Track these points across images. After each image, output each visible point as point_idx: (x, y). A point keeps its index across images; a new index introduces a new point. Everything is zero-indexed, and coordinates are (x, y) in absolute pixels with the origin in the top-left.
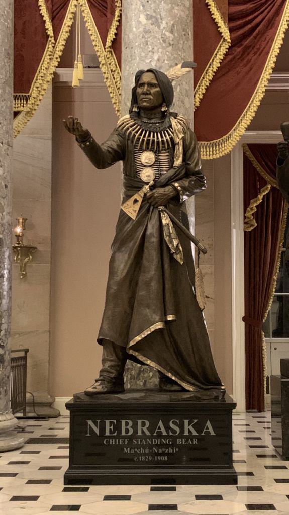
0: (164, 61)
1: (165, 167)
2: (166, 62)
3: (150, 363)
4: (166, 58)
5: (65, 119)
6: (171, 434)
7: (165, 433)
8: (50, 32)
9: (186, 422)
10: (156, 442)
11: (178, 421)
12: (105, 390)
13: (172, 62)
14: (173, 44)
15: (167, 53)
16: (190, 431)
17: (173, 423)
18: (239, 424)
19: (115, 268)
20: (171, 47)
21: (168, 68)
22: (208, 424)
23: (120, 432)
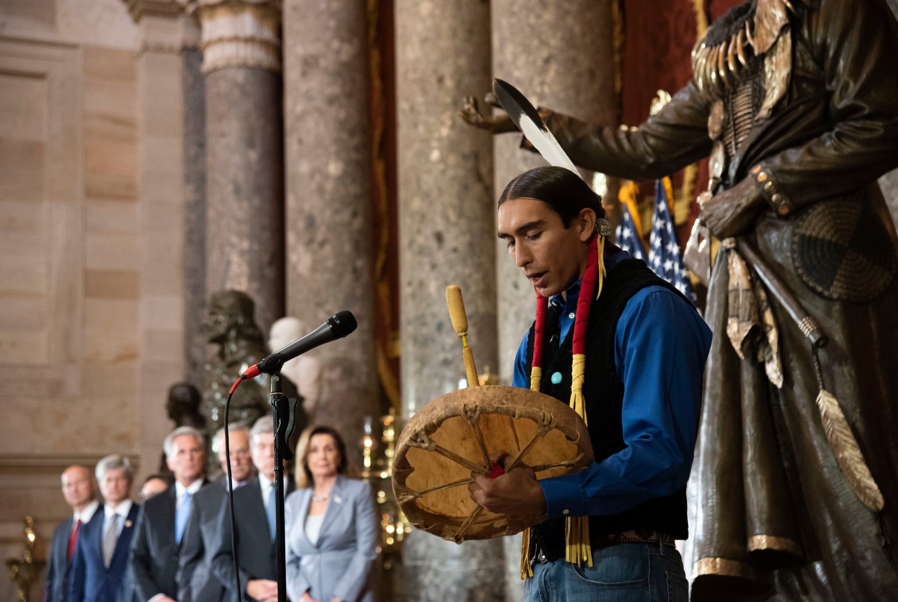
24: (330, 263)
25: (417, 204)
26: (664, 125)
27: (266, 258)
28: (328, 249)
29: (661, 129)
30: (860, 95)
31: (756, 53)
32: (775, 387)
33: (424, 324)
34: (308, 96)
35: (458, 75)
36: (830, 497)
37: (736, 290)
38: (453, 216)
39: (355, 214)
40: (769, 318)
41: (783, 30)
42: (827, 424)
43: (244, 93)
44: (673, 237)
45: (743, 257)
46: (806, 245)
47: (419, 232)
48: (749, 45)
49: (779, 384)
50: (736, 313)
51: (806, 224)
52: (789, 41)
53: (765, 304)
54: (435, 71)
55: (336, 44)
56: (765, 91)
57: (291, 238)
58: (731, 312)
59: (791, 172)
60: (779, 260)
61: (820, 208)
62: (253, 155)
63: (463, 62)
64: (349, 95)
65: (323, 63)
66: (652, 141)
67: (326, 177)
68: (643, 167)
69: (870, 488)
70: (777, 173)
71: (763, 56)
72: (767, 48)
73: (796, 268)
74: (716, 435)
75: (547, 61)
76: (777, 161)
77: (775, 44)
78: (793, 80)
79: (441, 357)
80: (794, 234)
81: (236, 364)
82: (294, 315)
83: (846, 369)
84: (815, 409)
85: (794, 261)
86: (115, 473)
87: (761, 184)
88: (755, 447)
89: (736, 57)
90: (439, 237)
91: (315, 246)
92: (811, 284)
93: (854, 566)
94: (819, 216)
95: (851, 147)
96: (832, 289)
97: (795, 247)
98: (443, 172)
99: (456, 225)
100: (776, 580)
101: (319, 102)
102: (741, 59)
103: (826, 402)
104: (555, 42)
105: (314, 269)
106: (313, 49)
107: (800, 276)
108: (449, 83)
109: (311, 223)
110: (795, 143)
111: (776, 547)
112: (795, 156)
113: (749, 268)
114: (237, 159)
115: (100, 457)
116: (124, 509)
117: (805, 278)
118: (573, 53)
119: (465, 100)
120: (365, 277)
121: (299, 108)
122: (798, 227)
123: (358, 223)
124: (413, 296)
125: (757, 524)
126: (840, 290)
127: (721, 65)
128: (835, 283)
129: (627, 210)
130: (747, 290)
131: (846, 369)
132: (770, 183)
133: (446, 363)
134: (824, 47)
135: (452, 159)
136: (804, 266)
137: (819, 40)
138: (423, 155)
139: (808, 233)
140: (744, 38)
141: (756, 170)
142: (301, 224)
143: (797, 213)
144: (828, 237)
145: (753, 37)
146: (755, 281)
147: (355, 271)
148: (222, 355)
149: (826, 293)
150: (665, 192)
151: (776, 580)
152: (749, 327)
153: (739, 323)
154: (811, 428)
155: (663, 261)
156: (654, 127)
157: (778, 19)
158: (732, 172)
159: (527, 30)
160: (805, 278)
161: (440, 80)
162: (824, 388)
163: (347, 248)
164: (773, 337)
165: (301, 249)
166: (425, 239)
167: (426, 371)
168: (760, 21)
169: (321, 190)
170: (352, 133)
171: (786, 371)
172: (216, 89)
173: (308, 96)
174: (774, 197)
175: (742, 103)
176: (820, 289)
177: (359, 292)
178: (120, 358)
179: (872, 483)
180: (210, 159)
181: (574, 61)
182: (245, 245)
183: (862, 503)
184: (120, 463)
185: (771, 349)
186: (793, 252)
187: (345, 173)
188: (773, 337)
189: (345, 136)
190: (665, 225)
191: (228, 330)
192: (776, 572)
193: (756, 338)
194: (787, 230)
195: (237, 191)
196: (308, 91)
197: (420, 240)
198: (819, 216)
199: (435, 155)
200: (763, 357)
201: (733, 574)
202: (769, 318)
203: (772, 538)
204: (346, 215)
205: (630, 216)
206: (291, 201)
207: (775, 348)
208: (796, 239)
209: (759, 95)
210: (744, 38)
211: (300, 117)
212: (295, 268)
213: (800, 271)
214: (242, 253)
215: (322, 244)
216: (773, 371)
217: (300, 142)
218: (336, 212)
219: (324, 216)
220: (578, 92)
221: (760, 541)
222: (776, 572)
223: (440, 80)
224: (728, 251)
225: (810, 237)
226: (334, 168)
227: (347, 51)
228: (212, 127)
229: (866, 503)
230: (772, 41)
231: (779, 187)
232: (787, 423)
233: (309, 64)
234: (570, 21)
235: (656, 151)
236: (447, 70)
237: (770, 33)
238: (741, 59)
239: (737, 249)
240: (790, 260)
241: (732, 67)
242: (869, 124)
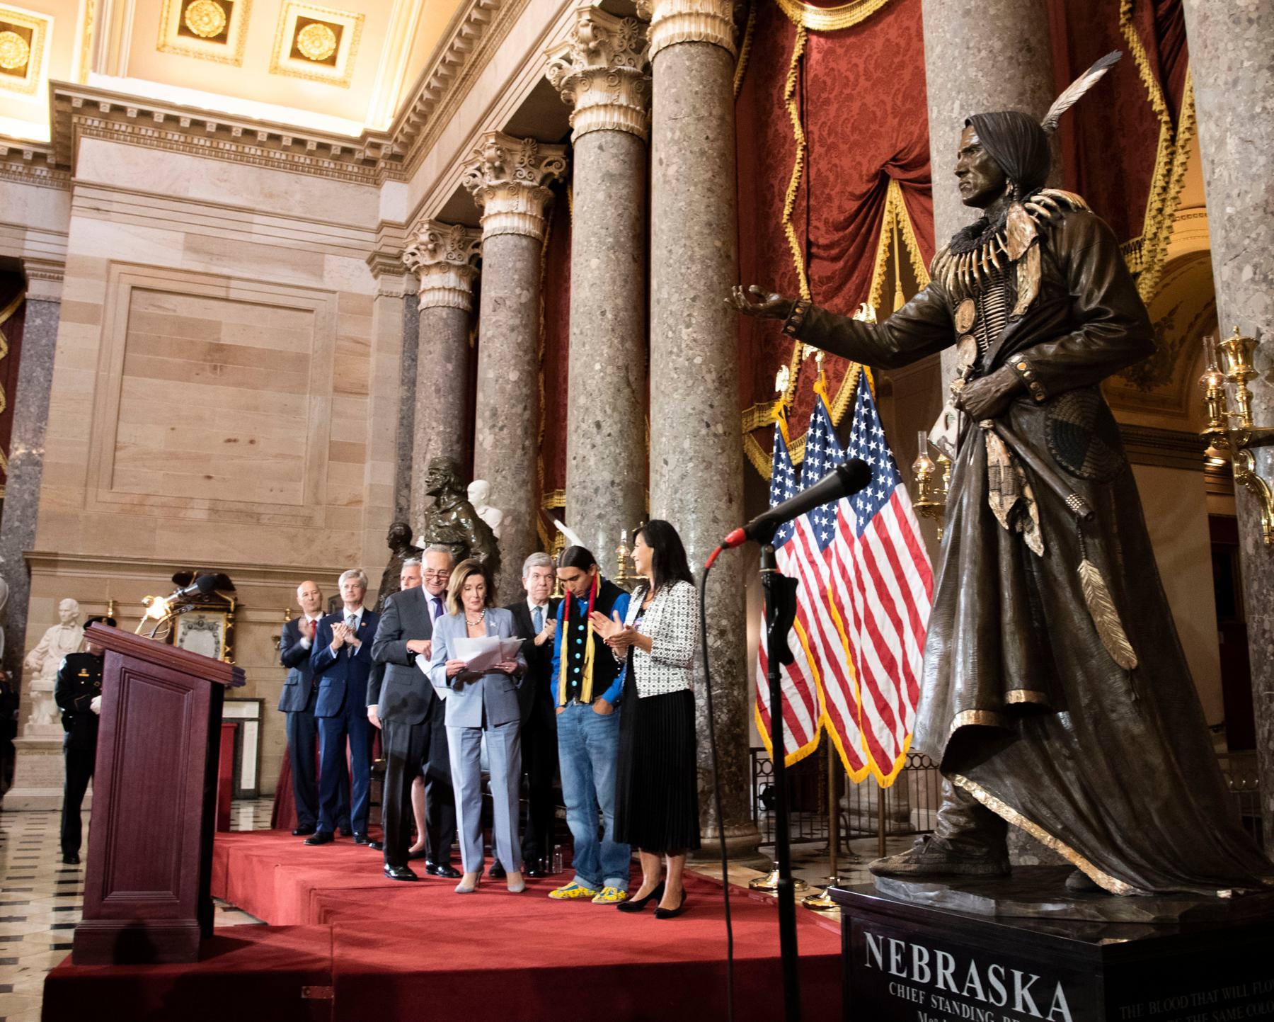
0: (1242, 63)
1: (997, 321)
2: (1246, 64)
3: (966, 783)
4: (1245, 54)
5: (780, 292)
6: (992, 1000)
7: (981, 997)
8: (1158, 105)
9: (1018, 975)
10: (927, 979)
11: (1002, 970)
12: (913, 867)
13: (1261, 57)
14: (1259, 18)
15: (1247, 44)
16: (1026, 1006)
17: (995, 971)
18: (245, 283)
19: (722, 473)
20: (1255, 25)
21: (1253, 75)
22: (1059, 992)
23: (910, 974)
24: (507, 442)
25: (582, 400)
26: (907, 320)
27: (455, 438)
28: (505, 431)
29: (904, 323)
30: (1104, 300)
31: (1010, 259)
32: (1036, 555)
33: (585, 488)
34: (497, 325)
35: (616, 309)
36: (1082, 655)
37: (997, 466)
38: (609, 411)
39: (525, 409)
40: (1028, 493)
41: (1034, 241)
42: (1088, 592)
43: (446, 324)
44: (877, 422)
45: (1001, 437)
46: (1059, 429)
47: (583, 420)
48: (1002, 251)
49: (1040, 554)
50: (997, 487)
51: (1057, 410)
52: (1038, 252)
53: (1024, 480)
54: (600, 307)
55: (518, 291)
56: (1017, 293)
57: (479, 423)
58: (991, 486)
59: (1048, 363)
60: (1034, 442)
61: (1069, 397)
62: (450, 367)
63: (619, 301)
64: (525, 326)
65: (508, 303)
66: (896, 334)
67: (507, 382)
68: (888, 356)
69: (1125, 649)
70: (1035, 364)
71: (1015, 262)
72: (1019, 256)
73: (1050, 449)
74: (976, 597)
75: (694, 299)
76: (1033, 351)
77: (1026, 253)
78: (1044, 284)
79: (597, 512)
80: (1047, 419)
81: (447, 511)
82: (479, 478)
83: (1097, 541)
84: (1075, 580)
85: (1048, 442)
86: (352, 582)
87: (1019, 373)
88: (1014, 609)
89: (990, 262)
90: (598, 425)
91: (497, 430)
92: (1064, 464)
93: (1101, 718)
94: (1069, 404)
95: (1098, 344)
96: (1083, 469)
97: (1048, 430)
98: (603, 378)
99: (610, 417)
100: (1021, 727)
101: (504, 330)
102: (995, 263)
103: (1088, 571)
104: (701, 286)
105: (495, 446)
106: (501, 294)
107: (1054, 456)
108: (609, 316)
109: (494, 414)
110: (1049, 339)
111: (1034, 701)
112: (1051, 349)
113: (1008, 447)
114: (438, 369)
115: (343, 571)
116: (359, 613)
117: (1058, 458)
118: (712, 295)
119: (734, 288)
120: (531, 453)
121: (490, 334)
122: (1051, 413)
123: (527, 415)
124: (577, 467)
125: (1016, 680)
126: (1089, 470)
127: (974, 269)
128: (1085, 464)
129: (820, 399)
130: (1009, 467)
131: (1097, 541)
132: (1028, 373)
133: (600, 516)
134: (1069, 259)
135: (610, 370)
136: (1057, 447)
137: (1063, 253)
138: (588, 366)
139: (1060, 418)
140: (997, 247)
141: (1015, 359)
142: (487, 414)
143: (1050, 401)
144: (1077, 423)
145: (1006, 246)
146: (1015, 458)
147: (523, 448)
148: (437, 504)
149: (1078, 472)
150: (869, 384)
151: (1021, 727)
152: (1014, 501)
153: (1001, 496)
154: (1067, 594)
155: (868, 442)
156: (898, 321)
157: (1028, 233)
158: (987, 362)
159: (680, 277)
160: (1058, 458)
161: (603, 313)
162: (1087, 558)
163: (519, 432)
164: (1033, 510)
165: (487, 431)
166: (588, 425)
167: (585, 522)
168: (1011, 233)
169: (502, 391)
170: (525, 351)
171: (1045, 541)
172: (424, 322)
173: (497, 325)
174: (1032, 386)
175: (994, 301)
176: (1072, 469)
177: (526, 463)
178: (349, 504)
179: (1127, 645)
180: (420, 369)
181: (713, 301)
182: (441, 428)
183: (1114, 662)
184: (357, 574)
185: (1031, 521)
186: (1046, 434)
187: (520, 379)
188: (1033, 510)
189: (521, 353)
190: (869, 412)
191: (444, 486)
192: (1021, 722)
193: (1019, 512)
194: (1040, 415)
195: (438, 391)
196: (497, 321)
197: (584, 426)
198: (1069, 404)
199: (598, 367)
200: (1022, 528)
201: (992, 725)
202: (1028, 493)
203: (1031, 692)
204: (519, 409)
205: (823, 404)
206: (480, 397)
207: (1036, 521)
208: (1049, 423)
209: (1011, 298)
210: (997, 247)
211: (489, 340)
212: (481, 444)
213: (1054, 452)
214: (438, 434)
215: (501, 429)
216: (1033, 540)
217: (489, 356)
218: (513, 406)
219: (504, 409)
220: (715, 323)
221: (1017, 696)
222: (1021, 722)
223: (603, 313)
224: (986, 431)
225: (1062, 421)
226: (513, 376)
227: (525, 296)
228: (422, 346)
229: (1119, 662)
230: (1022, 250)
231: (1036, 375)
232: (1039, 586)
233: (498, 303)
234: (710, 273)
235: (900, 342)
236: (608, 307)
237: (1020, 244)
238: (995, 263)
239: (995, 430)
240: (1044, 442)
241: (986, 270)
242: (1114, 326)
